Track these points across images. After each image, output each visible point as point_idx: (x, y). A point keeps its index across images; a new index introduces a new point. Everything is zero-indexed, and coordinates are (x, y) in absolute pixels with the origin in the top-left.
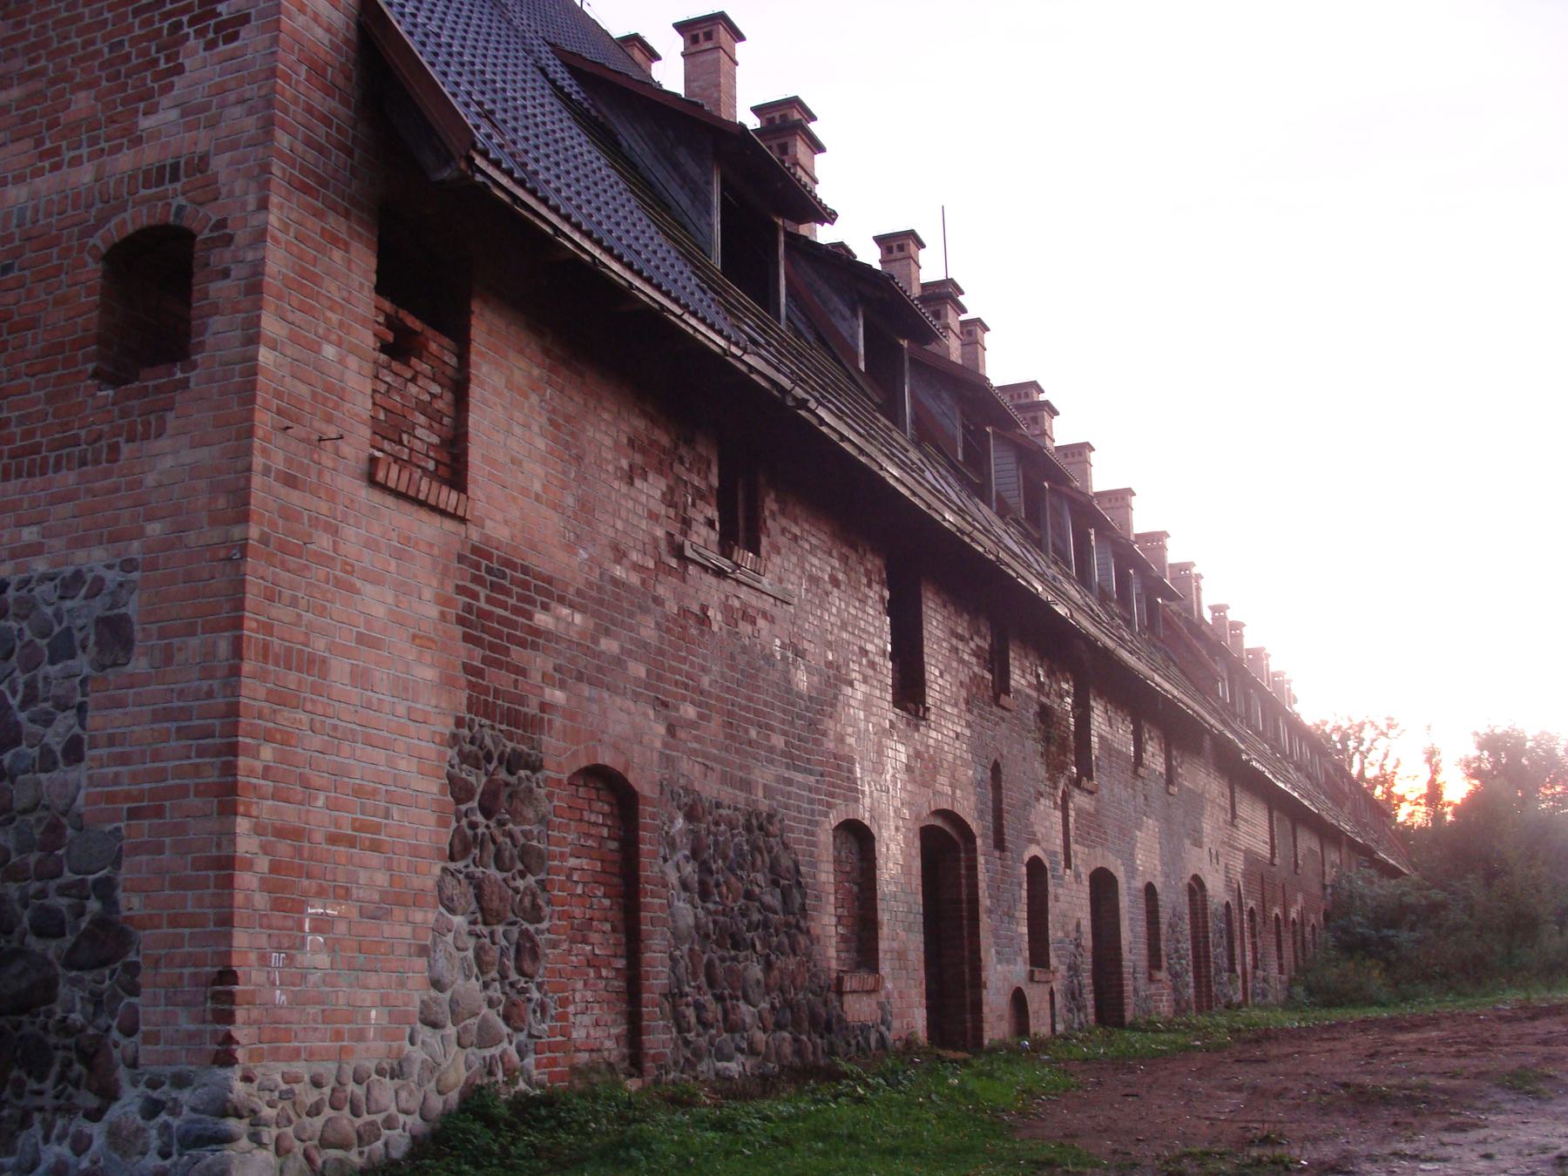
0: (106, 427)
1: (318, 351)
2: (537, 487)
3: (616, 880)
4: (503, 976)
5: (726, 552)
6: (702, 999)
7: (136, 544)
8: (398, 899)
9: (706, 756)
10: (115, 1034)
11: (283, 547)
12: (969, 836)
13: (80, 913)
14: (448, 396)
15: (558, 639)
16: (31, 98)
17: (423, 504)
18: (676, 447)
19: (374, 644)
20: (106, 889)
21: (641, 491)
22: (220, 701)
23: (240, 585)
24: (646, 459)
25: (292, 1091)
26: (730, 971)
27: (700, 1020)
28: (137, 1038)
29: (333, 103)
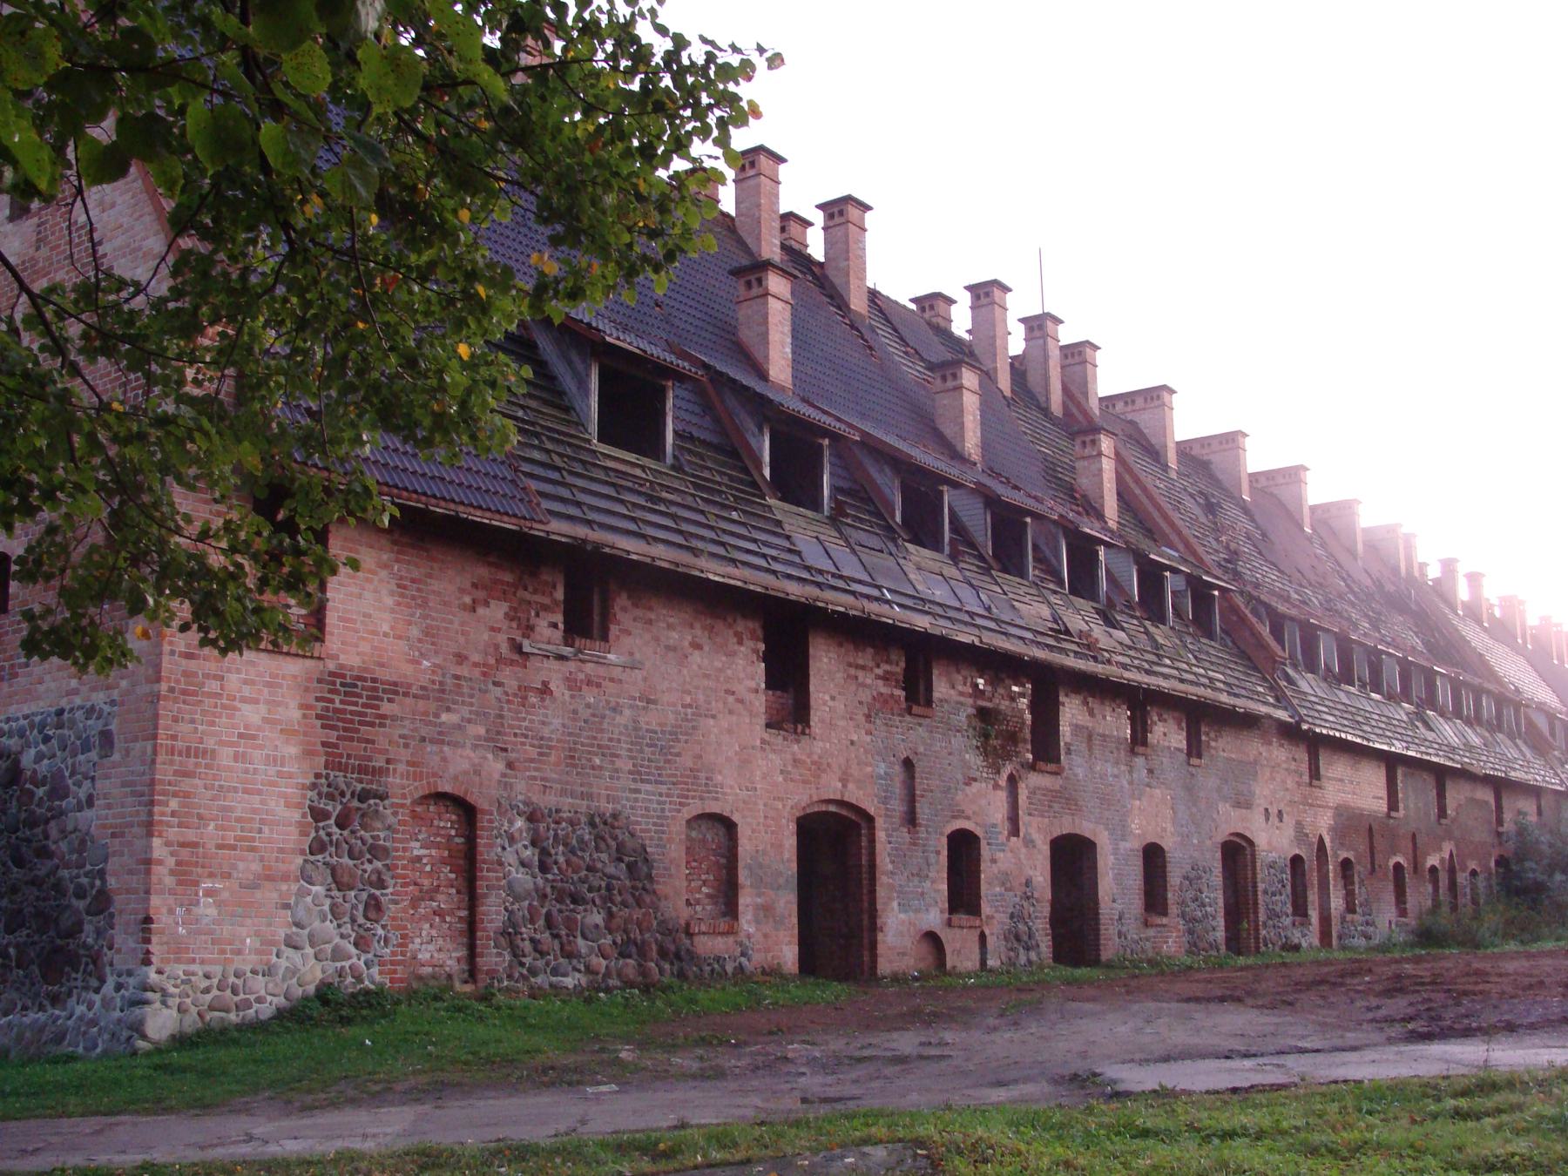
4: (353, 920)
12: (870, 819)
20: (102, 874)
22: (147, 778)
23: (156, 716)
24: (486, 592)
27: (536, 950)
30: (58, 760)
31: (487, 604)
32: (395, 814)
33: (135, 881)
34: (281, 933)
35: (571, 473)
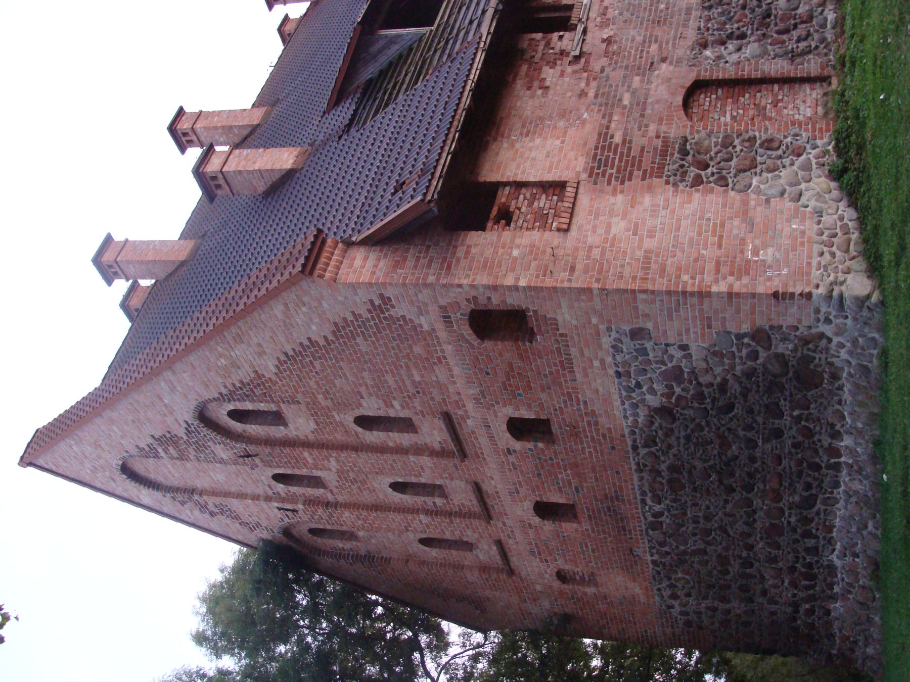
0: (553, 338)
1: (516, 258)
2: (558, 142)
3: (736, 90)
4: (780, 157)
5: (573, 28)
6: (795, 38)
7: (601, 327)
8: (744, 213)
9: (675, 39)
10: (798, 333)
11: (600, 272)
13: (749, 345)
14: (523, 190)
15: (626, 129)
16: (417, 367)
17: (574, 204)
18: (526, 60)
19: (636, 225)
20: (739, 337)
21: (551, 81)
23: (618, 291)
24: (535, 81)
25: (824, 266)
26: (782, 20)
27: (806, 39)
28: (799, 326)
29: (409, 255)
30: (654, 376)
31: (544, 80)
32: (698, 132)
33: (745, 307)
34: (789, 205)
35: (450, 34)
